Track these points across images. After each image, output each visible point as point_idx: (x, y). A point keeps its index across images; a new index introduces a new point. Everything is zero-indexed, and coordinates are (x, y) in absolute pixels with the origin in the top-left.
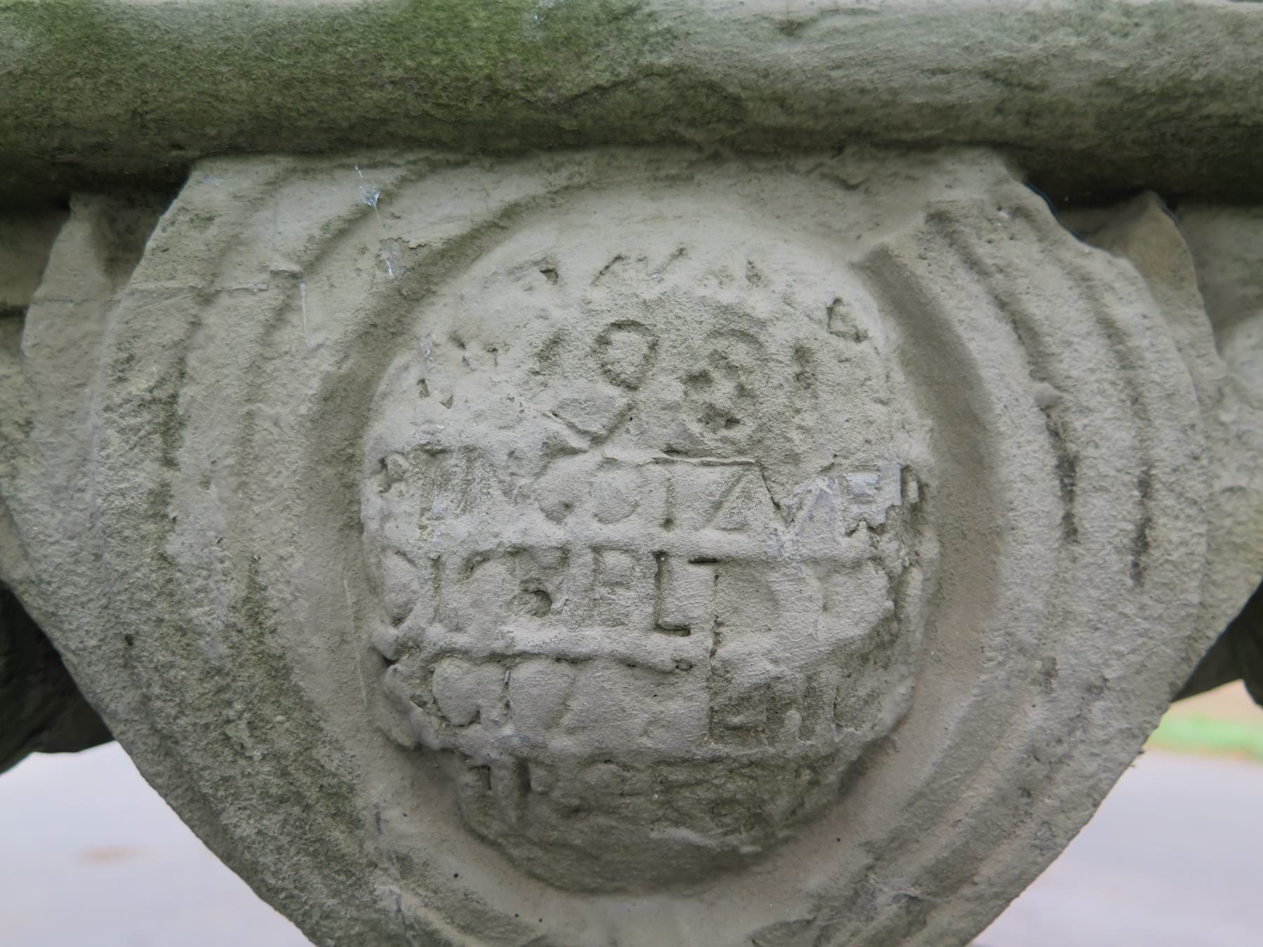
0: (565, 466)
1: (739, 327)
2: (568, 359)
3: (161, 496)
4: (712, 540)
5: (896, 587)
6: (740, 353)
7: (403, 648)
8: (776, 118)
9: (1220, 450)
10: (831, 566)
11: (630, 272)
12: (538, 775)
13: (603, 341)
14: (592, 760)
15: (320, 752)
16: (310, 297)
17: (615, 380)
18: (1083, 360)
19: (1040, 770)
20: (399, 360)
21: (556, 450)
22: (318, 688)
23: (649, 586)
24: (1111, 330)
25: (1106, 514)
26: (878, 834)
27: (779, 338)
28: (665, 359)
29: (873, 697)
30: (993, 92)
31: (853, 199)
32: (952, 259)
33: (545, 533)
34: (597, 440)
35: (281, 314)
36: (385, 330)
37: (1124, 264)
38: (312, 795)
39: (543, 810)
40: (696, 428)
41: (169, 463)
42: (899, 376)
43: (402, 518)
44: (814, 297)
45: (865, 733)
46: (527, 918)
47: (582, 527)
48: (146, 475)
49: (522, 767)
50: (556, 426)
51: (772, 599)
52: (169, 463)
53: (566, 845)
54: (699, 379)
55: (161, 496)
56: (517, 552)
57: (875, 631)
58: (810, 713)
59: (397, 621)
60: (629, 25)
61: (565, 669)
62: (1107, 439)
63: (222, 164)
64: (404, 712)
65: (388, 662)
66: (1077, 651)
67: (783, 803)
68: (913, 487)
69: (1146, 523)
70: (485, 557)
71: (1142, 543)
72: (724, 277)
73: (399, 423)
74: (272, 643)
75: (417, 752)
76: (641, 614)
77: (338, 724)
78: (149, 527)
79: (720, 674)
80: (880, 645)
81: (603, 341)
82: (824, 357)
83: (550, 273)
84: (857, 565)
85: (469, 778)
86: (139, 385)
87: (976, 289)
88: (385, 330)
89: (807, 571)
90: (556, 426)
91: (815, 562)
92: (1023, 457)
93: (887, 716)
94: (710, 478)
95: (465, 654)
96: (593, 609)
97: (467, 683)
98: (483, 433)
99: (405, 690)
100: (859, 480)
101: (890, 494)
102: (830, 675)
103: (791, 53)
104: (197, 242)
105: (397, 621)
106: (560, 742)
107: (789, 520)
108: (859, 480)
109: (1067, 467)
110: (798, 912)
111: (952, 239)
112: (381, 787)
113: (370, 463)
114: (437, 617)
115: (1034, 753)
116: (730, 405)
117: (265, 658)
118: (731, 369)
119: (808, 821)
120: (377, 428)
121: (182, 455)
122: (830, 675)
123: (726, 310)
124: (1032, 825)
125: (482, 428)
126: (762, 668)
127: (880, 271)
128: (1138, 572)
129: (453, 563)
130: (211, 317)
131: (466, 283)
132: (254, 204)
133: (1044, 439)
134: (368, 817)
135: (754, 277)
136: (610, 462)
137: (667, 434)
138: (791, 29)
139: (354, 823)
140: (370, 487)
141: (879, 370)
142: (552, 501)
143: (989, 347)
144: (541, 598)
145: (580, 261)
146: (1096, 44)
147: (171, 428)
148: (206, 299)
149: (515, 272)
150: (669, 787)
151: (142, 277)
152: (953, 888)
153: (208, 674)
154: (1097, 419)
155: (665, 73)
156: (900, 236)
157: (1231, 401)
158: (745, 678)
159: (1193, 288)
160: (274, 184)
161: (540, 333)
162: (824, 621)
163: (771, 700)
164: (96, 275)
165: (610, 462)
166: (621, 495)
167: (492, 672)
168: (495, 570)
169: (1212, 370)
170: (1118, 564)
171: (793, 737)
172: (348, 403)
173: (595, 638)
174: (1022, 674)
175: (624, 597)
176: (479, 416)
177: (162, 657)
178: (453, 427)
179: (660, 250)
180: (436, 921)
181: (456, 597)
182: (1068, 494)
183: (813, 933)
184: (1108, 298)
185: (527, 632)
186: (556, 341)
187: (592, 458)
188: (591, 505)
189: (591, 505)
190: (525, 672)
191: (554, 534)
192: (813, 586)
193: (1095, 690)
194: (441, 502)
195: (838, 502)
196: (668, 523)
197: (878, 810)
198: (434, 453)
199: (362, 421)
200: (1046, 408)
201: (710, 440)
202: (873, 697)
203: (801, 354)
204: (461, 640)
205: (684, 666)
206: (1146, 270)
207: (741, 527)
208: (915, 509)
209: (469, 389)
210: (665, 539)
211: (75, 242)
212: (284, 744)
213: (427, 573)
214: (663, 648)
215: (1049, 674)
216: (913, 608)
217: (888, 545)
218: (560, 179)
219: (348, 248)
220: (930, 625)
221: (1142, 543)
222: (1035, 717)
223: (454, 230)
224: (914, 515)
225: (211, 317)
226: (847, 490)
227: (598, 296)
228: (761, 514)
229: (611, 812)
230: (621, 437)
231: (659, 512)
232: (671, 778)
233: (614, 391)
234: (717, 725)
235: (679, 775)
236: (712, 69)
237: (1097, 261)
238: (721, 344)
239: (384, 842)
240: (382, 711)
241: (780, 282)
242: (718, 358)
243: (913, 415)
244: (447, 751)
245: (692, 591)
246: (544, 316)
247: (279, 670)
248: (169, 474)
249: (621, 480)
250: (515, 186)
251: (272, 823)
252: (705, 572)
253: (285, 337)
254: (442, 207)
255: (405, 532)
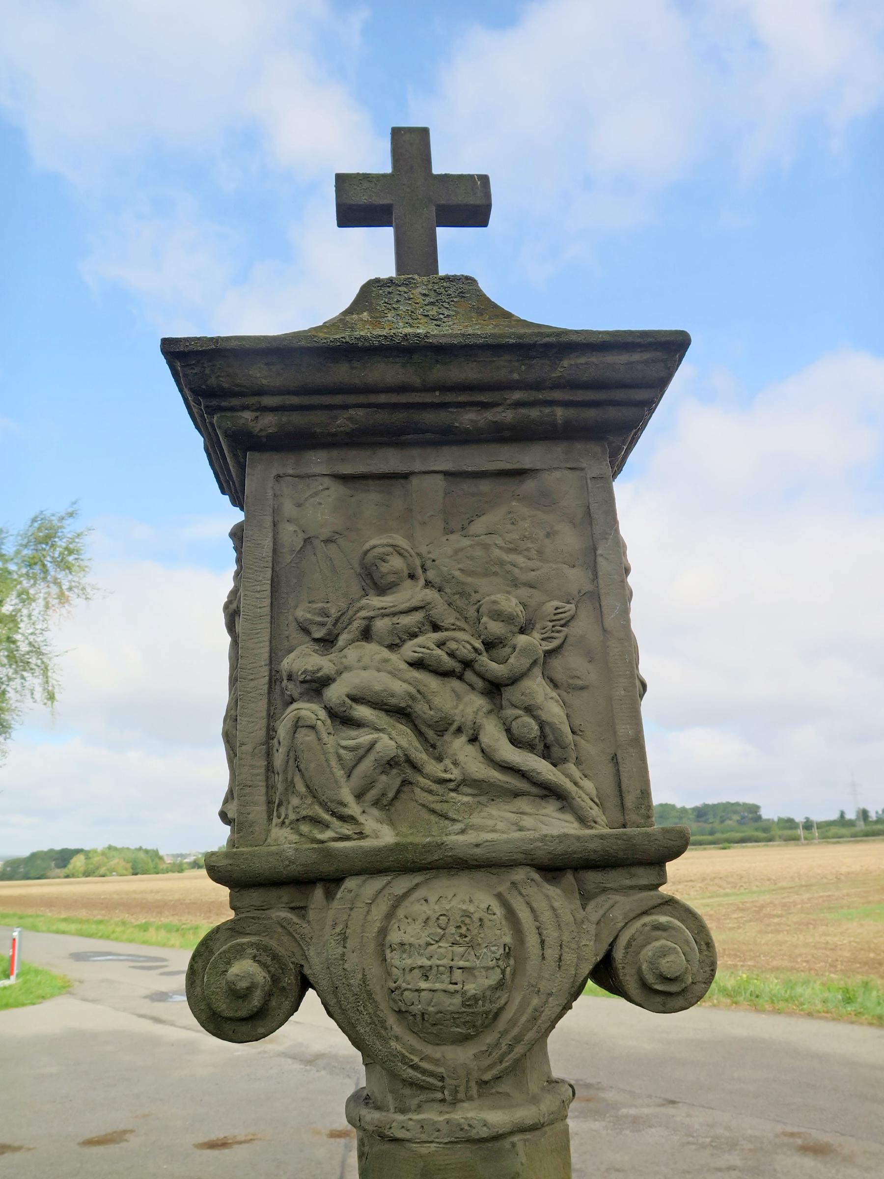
0: (431, 948)
1: (467, 914)
2: (431, 923)
3: (343, 955)
4: (462, 963)
5: (503, 972)
6: (467, 921)
7: (396, 988)
8: (476, 863)
9: (583, 935)
10: (487, 969)
11: (443, 901)
12: (426, 1016)
13: (438, 919)
14: (437, 1013)
15: (378, 1013)
16: (373, 907)
17: (441, 928)
18: (546, 916)
19: (538, 1014)
20: (393, 922)
21: (429, 944)
22: (378, 998)
23: (448, 974)
24: (554, 909)
25: (551, 953)
26: (501, 1029)
27: (476, 917)
28: (451, 922)
29: (499, 997)
30: (523, 856)
31: (494, 877)
32: (516, 893)
33: (428, 963)
34: (437, 942)
35: (368, 912)
36: (390, 915)
37: (558, 891)
38: (377, 1022)
39: (427, 1025)
40: (458, 938)
41: (345, 947)
42: (504, 922)
43: (395, 958)
44: (484, 906)
45: (497, 1006)
46: (424, 1050)
47: (435, 961)
48: (340, 950)
49: (423, 1014)
50: (428, 939)
51: (475, 976)
52: (345, 947)
53: (432, 1033)
54: (458, 927)
55: (343, 955)
56: (421, 967)
57: (498, 982)
58: (484, 1001)
59: (395, 982)
60: (442, 847)
61: (433, 994)
62: (552, 934)
63: (353, 877)
64: (397, 1003)
65: (393, 992)
66: (544, 986)
67: (480, 1022)
68: (507, 950)
69: (561, 956)
70: (414, 968)
71: (560, 960)
72: (464, 902)
73: (394, 937)
74: (368, 988)
75: (400, 1012)
76: (447, 980)
77: (383, 1006)
78: (341, 962)
79: (464, 993)
80: (500, 985)
81: (438, 919)
82: (486, 920)
83: (426, 901)
84: (493, 968)
85: (411, 1018)
86: (338, 930)
87: (522, 900)
88: (390, 915)
89: (482, 970)
90: (428, 939)
91: (484, 968)
92: (532, 940)
93: (503, 1001)
94: (462, 949)
95: (410, 990)
96: (437, 980)
97: (410, 996)
98: (412, 940)
99: (397, 998)
100: (493, 949)
101: (501, 951)
102: (488, 993)
103: (478, 851)
104: (349, 896)
105: (395, 982)
106: (431, 1009)
107: (478, 959)
108: (493, 949)
109: (543, 942)
110: (485, 1048)
111: (517, 888)
112: (392, 1020)
113: (387, 945)
114: (404, 982)
115: (536, 1010)
116: (465, 932)
117: (367, 991)
118: (466, 924)
119: (486, 1027)
120: (389, 938)
121: (347, 945)
122: (488, 993)
123: (464, 911)
124: (536, 1027)
125: (412, 939)
126: (473, 992)
127: (500, 897)
128: (559, 967)
129: (407, 970)
130: (352, 913)
131: (406, 903)
132: (360, 886)
133: (537, 936)
134: (389, 1027)
135: (471, 901)
136: (440, 947)
137: (452, 940)
138: (477, 845)
139: (386, 1029)
140: (388, 951)
141: (498, 922)
142: (428, 956)
143: (524, 915)
144: (426, 977)
145: (432, 899)
146: (545, 845)
147: (345, 939)
148: (351, 909)
149: (418, 901)
150: (454, 1018)
151: (335, 904)
152: (519, 1042)
153: (353, 995)
154: (549, 931)
155: (450, 856)
156: (503, 888)
157: (586, 922)
158: (470, 994)
159: (578, 896)
160: (364, 881)
161: (424, 917)
162: (486, 981)
163: (475, 998)
164: (325, 902)
165: (440, 947)
166: (442, 954)
167: (416, 993)
168: (416, 971)
169: (580, 914)
170: (554, 965)
171: (480, 1007)
172: (383, 932)
173: (438, 986)
174: (533, 991)
175: (444, 976)
176: (412, 936)
177: (344, 992)
178: (406, 939)
179: (450, 896)
180: (404, 1052)
181: (408, 977)
182: (543, 949)
183: (488, 1053)
184: (553, 901)
185: (423, 985)
186: (428, 919)
187: (436, 946)
188: (436, 956)
189: (436, 956)
190: (423, 994)
191: (429, 963)
192: (484, 973)
193: (550, 994)
194: (404, 956)
195: (489, 954)
196: (452, 960)
197: (502, 1024)
198: (402, 944)
199: (386, 936)
200: (538, 928)
201: (461, 941)
202: (499, 997)
203: (481, 920)
204: (409, 987)
205: (456, 992)
206: (564, 891)
207: (468, 961)
208: (508, 953)
209: (409, 930)
210: (452, 963)
211: (318, 893)
212: (371, 1011)
213: (402, 971)
214: (452, 988)
215: (539, 991)
216: (508, 976)
217: (501, 963)
218: (428, 876)
219: (382, 894)
220: (513, 981)
221: (560, 960)
222: (535, 1001)
223: (404, 890)
224: (508, 955)
225: (352, 913)
226: (491, 951)
227: (437, 907)
228: (472, 957)
229: (442, 1025)
230: (442, 941)
231: (451, 958)
232: (455, 1017)
233: (440, 931)
234: (464, 1004)
235: (456, 1016)
236: (461, 855)
237: (552, 891)
238: (463, 918)
239: (392, 1033)
240: (391, 1002)
241: (476, 903)
242: (463, 922)
243: (507, 931)
244: (406, 1011)
245: (458, 975)
246: (425, 912)
247: (369, 994)
248: (345, 950)
249: (442, 950)
250: (418, 878)
251: (368, 1029)
252: (460, 971)
253: (369, 917)
254: (402, 884)
255: (396, 962)
